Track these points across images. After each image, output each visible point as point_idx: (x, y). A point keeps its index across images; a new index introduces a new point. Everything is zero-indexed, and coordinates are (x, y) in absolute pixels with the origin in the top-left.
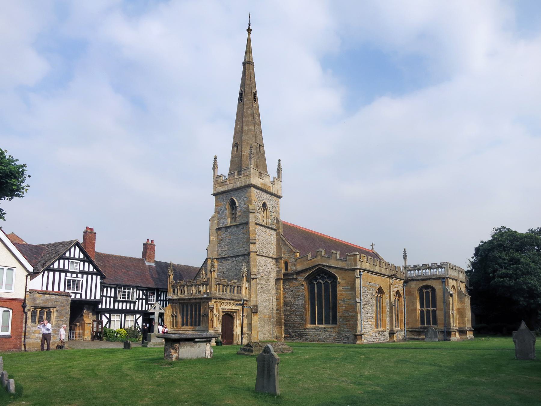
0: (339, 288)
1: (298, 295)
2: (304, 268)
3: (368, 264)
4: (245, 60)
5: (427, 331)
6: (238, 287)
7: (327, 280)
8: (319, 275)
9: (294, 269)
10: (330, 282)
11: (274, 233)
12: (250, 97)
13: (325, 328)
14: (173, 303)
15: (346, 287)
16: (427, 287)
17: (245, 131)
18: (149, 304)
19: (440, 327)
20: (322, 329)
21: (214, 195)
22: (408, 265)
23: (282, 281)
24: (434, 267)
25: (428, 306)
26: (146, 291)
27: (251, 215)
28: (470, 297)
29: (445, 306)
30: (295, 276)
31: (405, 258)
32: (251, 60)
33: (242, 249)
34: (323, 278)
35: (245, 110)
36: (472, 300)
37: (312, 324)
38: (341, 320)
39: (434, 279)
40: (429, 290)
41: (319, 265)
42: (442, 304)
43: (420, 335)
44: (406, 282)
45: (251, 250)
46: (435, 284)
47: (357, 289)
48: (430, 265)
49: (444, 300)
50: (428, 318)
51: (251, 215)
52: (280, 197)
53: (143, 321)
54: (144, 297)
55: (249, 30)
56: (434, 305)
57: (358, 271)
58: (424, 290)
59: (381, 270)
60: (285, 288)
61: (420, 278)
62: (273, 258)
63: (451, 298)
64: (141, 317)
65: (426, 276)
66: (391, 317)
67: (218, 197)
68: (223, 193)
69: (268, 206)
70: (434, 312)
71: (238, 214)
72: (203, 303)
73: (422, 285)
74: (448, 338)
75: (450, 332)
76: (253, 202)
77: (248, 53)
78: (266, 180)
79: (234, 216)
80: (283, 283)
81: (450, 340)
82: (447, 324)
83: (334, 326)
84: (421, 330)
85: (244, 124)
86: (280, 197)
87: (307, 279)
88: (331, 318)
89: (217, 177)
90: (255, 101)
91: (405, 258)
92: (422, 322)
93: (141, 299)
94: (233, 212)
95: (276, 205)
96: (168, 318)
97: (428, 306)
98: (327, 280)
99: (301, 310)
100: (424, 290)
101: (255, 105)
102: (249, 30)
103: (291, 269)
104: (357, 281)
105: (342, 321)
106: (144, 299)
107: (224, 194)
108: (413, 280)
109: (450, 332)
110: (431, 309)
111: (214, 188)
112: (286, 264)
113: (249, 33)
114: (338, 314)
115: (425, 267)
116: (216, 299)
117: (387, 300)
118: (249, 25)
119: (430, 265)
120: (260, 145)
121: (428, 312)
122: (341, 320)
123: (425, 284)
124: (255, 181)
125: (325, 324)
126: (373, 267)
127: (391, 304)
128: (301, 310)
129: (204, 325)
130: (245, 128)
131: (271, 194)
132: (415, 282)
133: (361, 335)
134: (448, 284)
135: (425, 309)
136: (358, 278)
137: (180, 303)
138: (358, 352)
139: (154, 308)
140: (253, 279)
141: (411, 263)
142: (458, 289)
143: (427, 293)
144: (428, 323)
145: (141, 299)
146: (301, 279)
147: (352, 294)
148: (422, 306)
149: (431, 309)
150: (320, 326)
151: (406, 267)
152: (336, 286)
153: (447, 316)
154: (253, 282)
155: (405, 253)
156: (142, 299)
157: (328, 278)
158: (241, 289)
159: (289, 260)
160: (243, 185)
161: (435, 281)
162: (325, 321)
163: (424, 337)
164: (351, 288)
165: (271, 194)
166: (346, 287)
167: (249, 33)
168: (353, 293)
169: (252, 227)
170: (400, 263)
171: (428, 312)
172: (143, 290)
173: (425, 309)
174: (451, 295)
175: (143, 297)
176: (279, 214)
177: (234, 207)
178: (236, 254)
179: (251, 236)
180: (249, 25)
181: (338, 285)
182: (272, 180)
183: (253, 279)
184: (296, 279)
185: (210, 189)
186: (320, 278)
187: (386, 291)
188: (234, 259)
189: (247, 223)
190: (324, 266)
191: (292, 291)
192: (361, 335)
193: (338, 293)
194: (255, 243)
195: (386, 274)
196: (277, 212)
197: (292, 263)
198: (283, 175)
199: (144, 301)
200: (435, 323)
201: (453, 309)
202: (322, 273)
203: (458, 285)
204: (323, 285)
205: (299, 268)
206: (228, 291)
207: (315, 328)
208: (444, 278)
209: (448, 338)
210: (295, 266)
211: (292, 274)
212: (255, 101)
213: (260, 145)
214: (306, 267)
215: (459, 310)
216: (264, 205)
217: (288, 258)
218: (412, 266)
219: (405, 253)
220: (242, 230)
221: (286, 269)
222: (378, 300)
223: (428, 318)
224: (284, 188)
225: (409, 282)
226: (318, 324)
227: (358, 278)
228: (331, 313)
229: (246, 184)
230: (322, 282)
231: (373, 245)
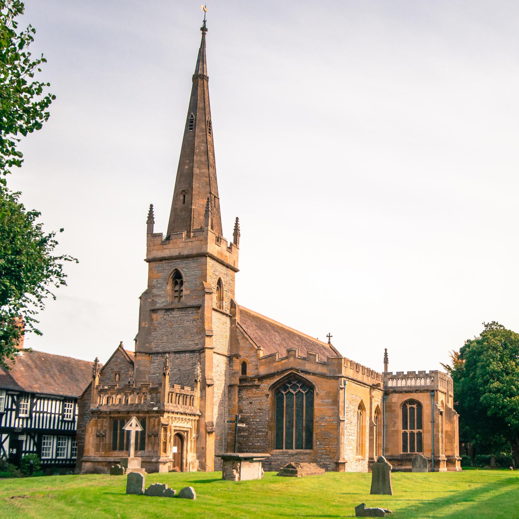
0: (317, 401)
1: (259, 409)
2: (269, 372)
3: (352, 371)
4: (197, 71)
5: (415, 459)
6: (191, 396)
7: (301, 390)
8: (290, 383)
9: (253, 372)
10: (304, 393)
11: (228, 320)
12: (204, 126)
13: (296, 454)
14: (99, 418)
15: (327, 401)
16: (412, 401)
17: (197, 174)
18: (20, 418)
19: (426, 454)
20: (293, 455)
21: (148, 261)
22: (389, 371)
23: (237, 389)
24: (421, 376)
25: (412, 427)
26: (18, 397)
27: (207, 296)
28: (459, 415)
29: (433, 427)
30: (256, 383)
31: (386, 361)
32: (205, 74)
33: (190, 343)
34: (294, 387)
35: (196, 144)
36: (460, 419)
37: (277, 448)
38: (318, 443)
39: (421, 392)
40: (415, 406)
41: (291, 369)
42: (430, 424)
43: (401, 465)
44: (387, 393)
45: (206, 346)
46: (424, 399)
47: (341, 404)
48: (417, 373)
49: (433, 419)
50: (412, 442)
51: (207, 296)
52: (236, 271)
53: (11, 446)
54: (14, 407)
55: (204, 29)
56: (420, 426)
57: (343, 379)
58: (409, 406)
59: (363, 378)
60: (240, 399)
61: (404, 389)
62: (226, 356)
63: (440, 416)
64: (8, 439)
65: (411, 387)
66: (371, 440)
67: (154, 264)
68: (162, 259)
69: (224, 283)
70: (420, 434)
71: (185, 292)
72: (150, 417)
73: (406, 399)
74: (435, 469)
75: (439, 461)
76: (208, 277)
77: (201, 63)
78: (224, 247)
79: (177, 294)
80: (239, 392)
81: (438, 471)
82: (435, 452)
83: (308, 451)
84: (404, 458)
85: (195, 165)
86: (236, 271)
87: (272, 387)
88: (304, 441)
89: (151, 235)
90: (210, 133)
91: (386, 361)
92: (405, 449)
93: (9, 410)
94: (177, 288)
95: (231, 282)
96: (91, 439)
97: (412, 427)
98: (301, 390)
99: (264, 430)
100: (409, 406)
101: (209, 139)
102: (204, 29)
103: (251, 372)
104: (341, 392)
105: (320, 444)
106: (14, 410)
107: (164, 262)
108: (395, 392)
109: (439, 461)
110: (416, 431)
111: (148, 251)
112: (244, 365)
113: (204, 34)
114: (314, 435)
115: (411, 375)
116: (169, 412)
117: (368, 419)
118: (205, 22)
119: (417, 373)
120: (215, 197)
121: (412, 434)
122: (318, 443)
123: (409, 398)
124: (212, 249)
125: (296, 448)
126: (356, 374)
127: (371, 423)
128: (264, 430)
129: (150, 449)
130: (196, 171)
131: (227, 266)
132: (397, 395)
133: (344, 463)
134: (437, 400)
135: (408, 431)
136: (342, 389)
137: (111, 417)
138: (242, 510)
139: (131, 425)
140: (209, 386)
141: (393, 369)
142: (446, 405)
143: (412, 409)
144: (412, 449)
145: (9, 410)
146: (266, 385)
147: (333, 409)
148: (405, 427)
149: (416, 431)
150: (290, 451)
151: (386, 374)
152: (313, 398)
153: (435, 440)
154: (208, 390)
155: (386, 354)
156: (12, 410)
157: (301, 387)
158: (193, 398)
159: (248, 360)
160: (195, 252)
161: (422, 394)
162: (296, 445)
163: (411, 467)
164: (333, 401)
165: (227, 266)
166: (327, 401)
167: (204, 34)
168: (336, 407)
169: (207, 312)
170: (380, 369)
171: (412, 434)
172: (12, 396)
173: (408, 431)
174: (441, 413)
175: (12, 406)
176: (234, 294)
177: (179, 281)
178: (180, 348)
179: (206, 327)
180: (205, 22)
181: (315, 397)
182: (229, 246)
183: (209, 386)
184: (258, 387)
185: (141, 250)
186: (291, 387)
187: (367, 406)
188: (178, 355)
189: (199, 307)
190: (297, 370)
191: (251, 403)
192: (344, 463)
193: (316, 407)
194: (211, 336)
195: (367, 383)
196: (233, 292)
197: (254, 363)
198: (241, 240)
199: (14, 413)
200: (420, 449)
201: (442, 432)
202: (294, 381)
203: (445, 399)
204: (285, 396)
205: (263, 371)
206: (181, 402)
207: (283, 454)
208: (433, 391)
209: (435, 469)
210: (257, 369)
211: (252, 379)
212: (210, 133)
213: (215, 197)
214: (273, 371)
215: (446, 432)
216: (219, 282)
217: (247, 357)
218: (394, 374)
219: (386, 354)
220: (192, 315)
221: (244, 371)
222: (360, 416)
223: (412, 442)
224: (243, 258)
225: (391, 395)
226: (286, 448)
227: (342, 389)
228: (304, 434)
229: (199, 251)
230: (294, 393)
231: (329, 336)
